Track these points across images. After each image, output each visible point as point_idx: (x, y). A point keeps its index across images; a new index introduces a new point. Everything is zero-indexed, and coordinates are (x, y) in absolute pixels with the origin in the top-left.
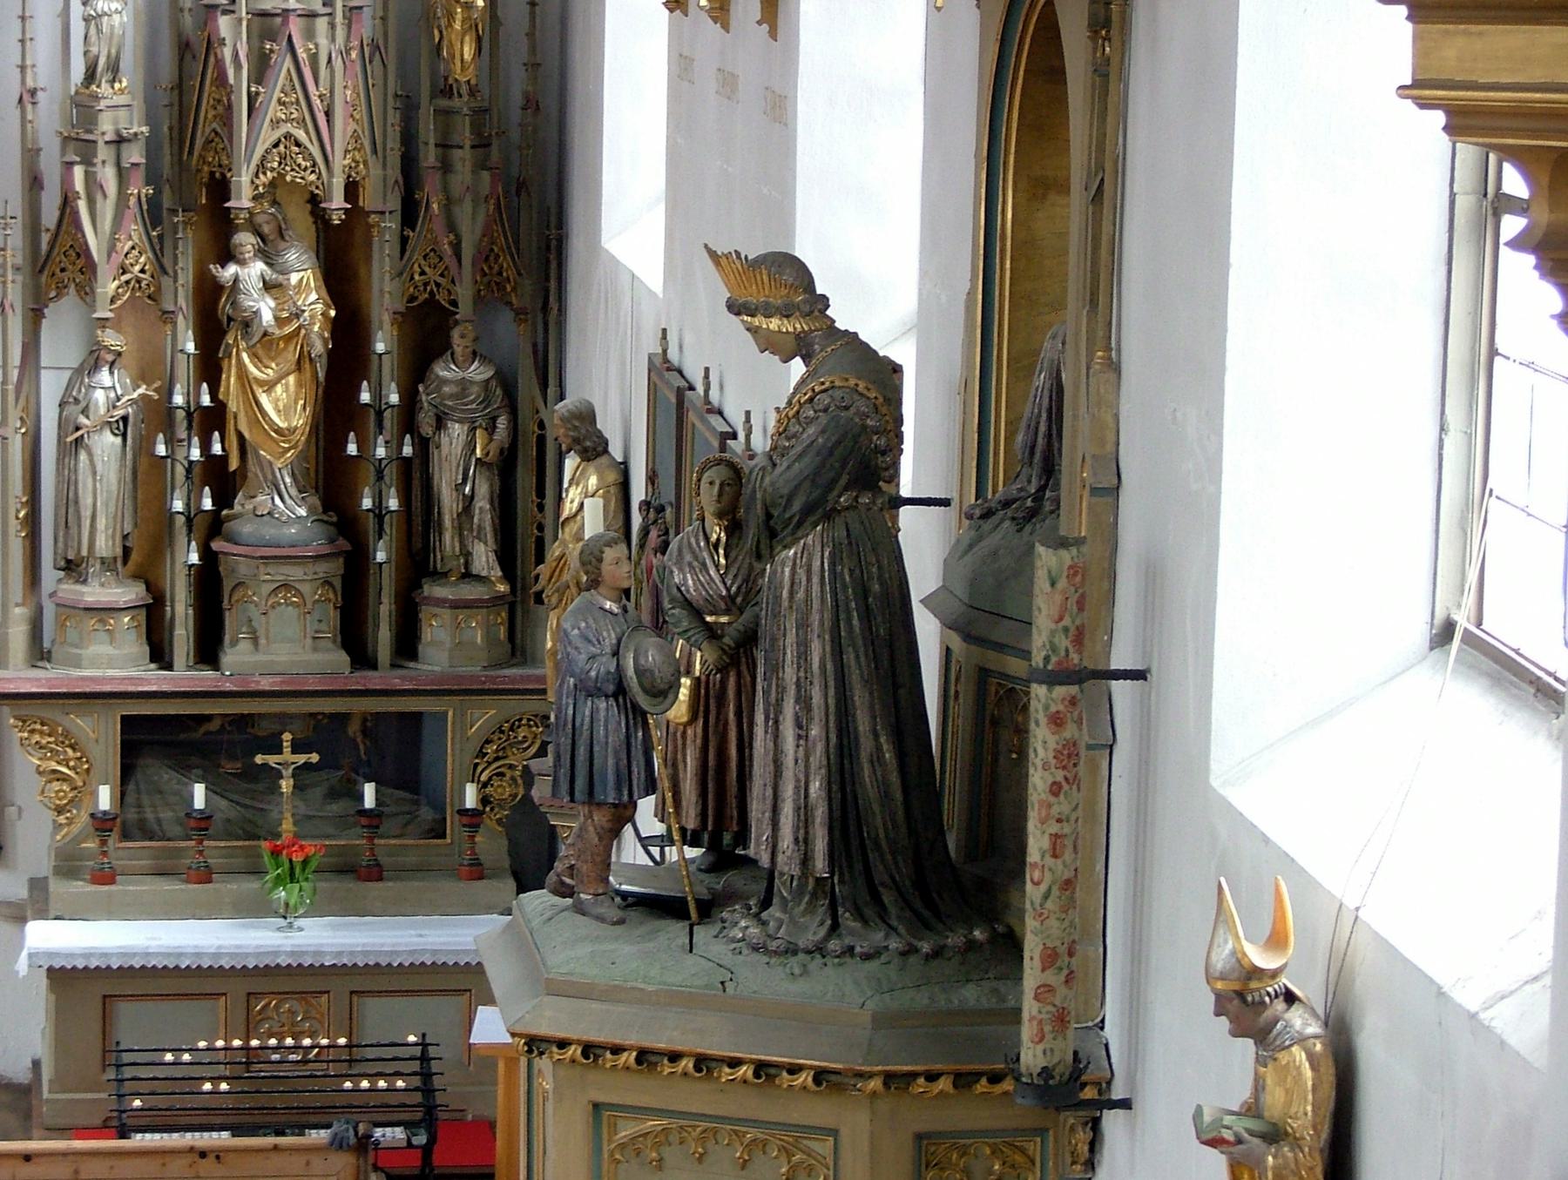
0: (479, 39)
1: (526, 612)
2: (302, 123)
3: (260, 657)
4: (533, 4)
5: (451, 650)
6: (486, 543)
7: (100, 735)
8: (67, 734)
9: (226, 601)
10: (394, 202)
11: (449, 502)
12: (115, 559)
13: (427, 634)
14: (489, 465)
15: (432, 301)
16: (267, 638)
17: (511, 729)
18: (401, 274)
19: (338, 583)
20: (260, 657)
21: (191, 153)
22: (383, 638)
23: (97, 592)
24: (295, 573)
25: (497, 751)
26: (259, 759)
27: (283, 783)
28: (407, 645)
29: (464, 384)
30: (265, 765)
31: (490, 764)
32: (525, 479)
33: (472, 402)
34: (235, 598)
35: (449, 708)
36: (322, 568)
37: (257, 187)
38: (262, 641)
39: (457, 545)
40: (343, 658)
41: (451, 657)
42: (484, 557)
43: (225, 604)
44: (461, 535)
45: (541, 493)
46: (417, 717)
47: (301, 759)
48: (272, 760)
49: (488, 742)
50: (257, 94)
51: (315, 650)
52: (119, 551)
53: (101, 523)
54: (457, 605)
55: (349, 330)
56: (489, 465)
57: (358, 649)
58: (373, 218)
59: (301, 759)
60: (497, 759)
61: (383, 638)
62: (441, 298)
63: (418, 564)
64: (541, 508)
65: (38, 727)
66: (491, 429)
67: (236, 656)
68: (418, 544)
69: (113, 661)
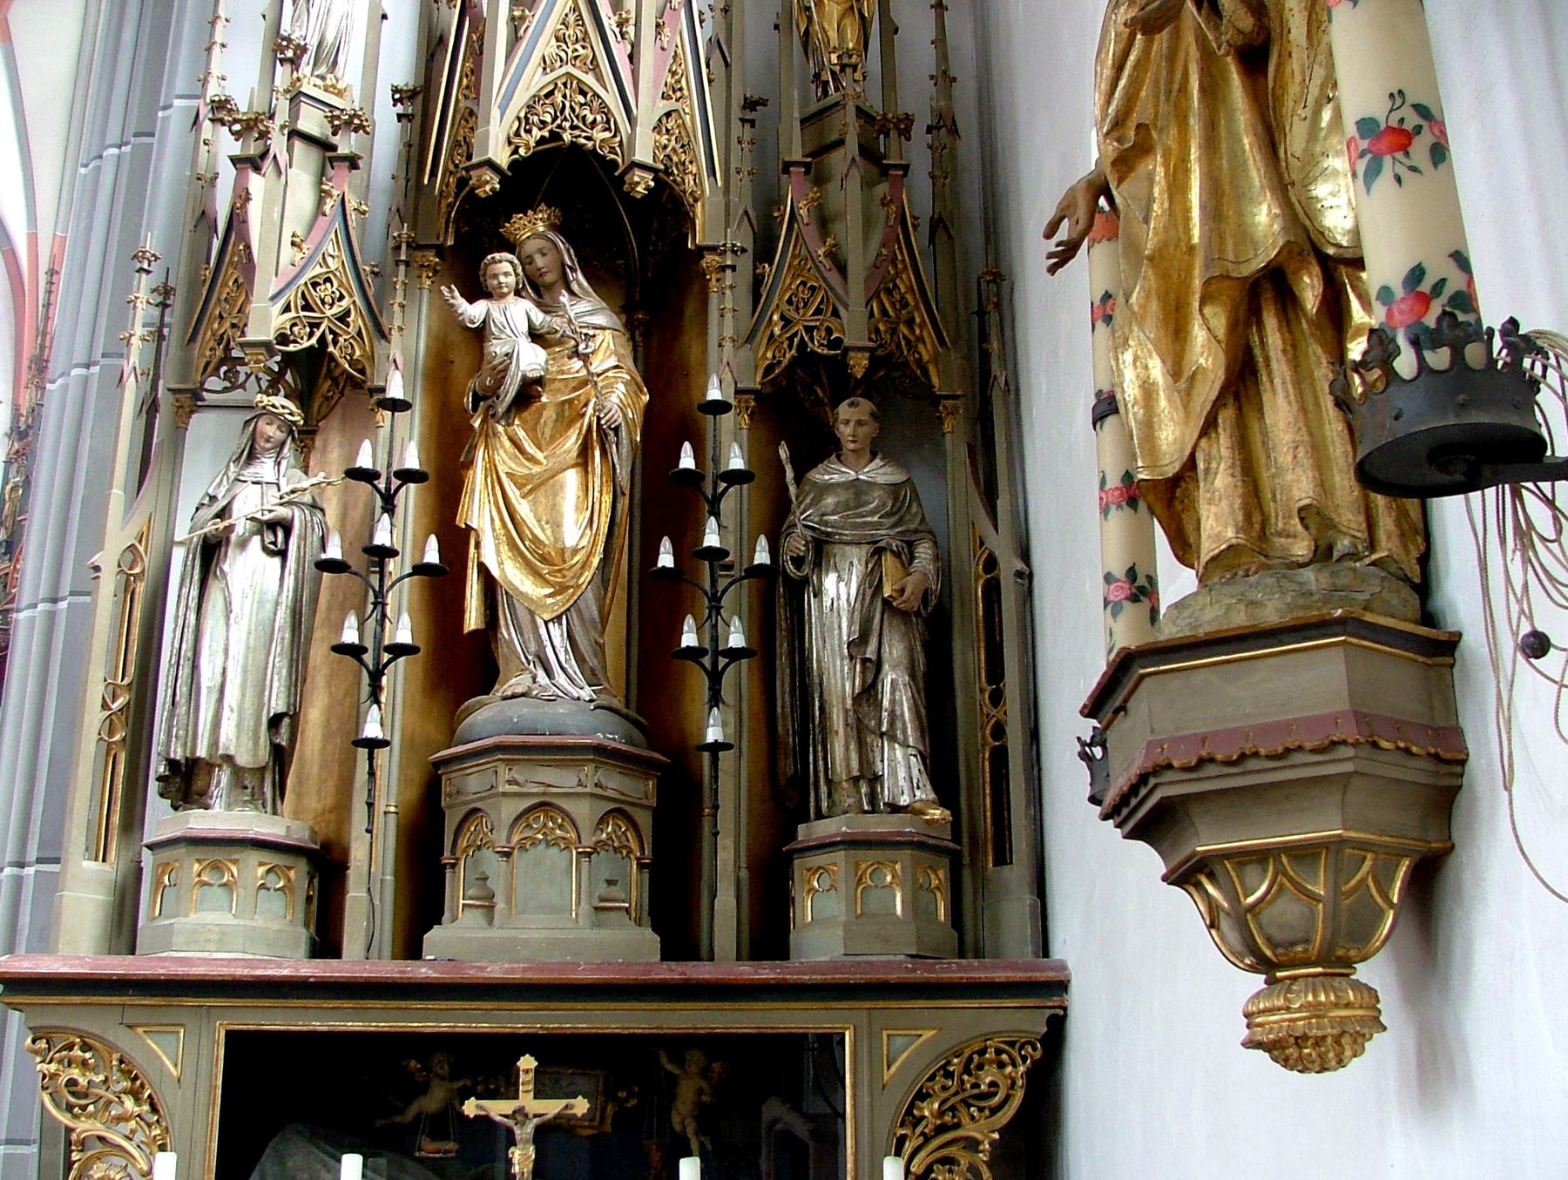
0: (864, 23)
1: (981, 881)
2: (594, 67)
3: (494, 933)
4: (939, 7)
5: (846, 925)
6: (905, 745)
7: (185, 1063)
8: (127, 1068)
9: (447, 853)
10: (741, 237)
11: (838, 677)
12: (261, 770)
13: (806, 909)
14: (904, 615)
15: (805, 357)
16: (509, 901)
17: (967, 1070)
18: (750, 339)
19: (645, 820)
20: (494, 933)
21: (433, 174)
22: (725, 909)
23: (221, 816)
24: (562, 779)
25: (941, 1113)
26: (471, 1107)
27: (516, 1154)
28: (769, 929)
29: (858, 489)
30: (484, 1121)
31: (927, 1139)
32: (967, 657)
33: (872, 513)
34: (462, 843)
35: (847, 1025)
36: (616, 782)
37: (515, 151)
38: (500, 905)
39: (854, 756)
40: (648, 941)
41: (848, 937)
42: (902, 771)
43: (446, 858)
44: (861, 745)
45: (995, 671)
46: (793, 1043)
47: (551, 1107)
48: (498, 1109)
49: (922, 1096)
50: (522, 18)
51: (597, 925)
52: (264, 755)
53: (232, 697)
54: (852, 843)
55: (671, 416)
56: (904, 615)
57: (674, 911)
58: (709, 260)
59: (551, 1107)
60: (941, 1129)
61: (725, 909)
62: (817, 346)
63: (787, 795)
64: (997, 698)
65: (77, 1052)
66: (906, 556)
67: (457, 942)
68: (788, 767)
69: (232, 927)
